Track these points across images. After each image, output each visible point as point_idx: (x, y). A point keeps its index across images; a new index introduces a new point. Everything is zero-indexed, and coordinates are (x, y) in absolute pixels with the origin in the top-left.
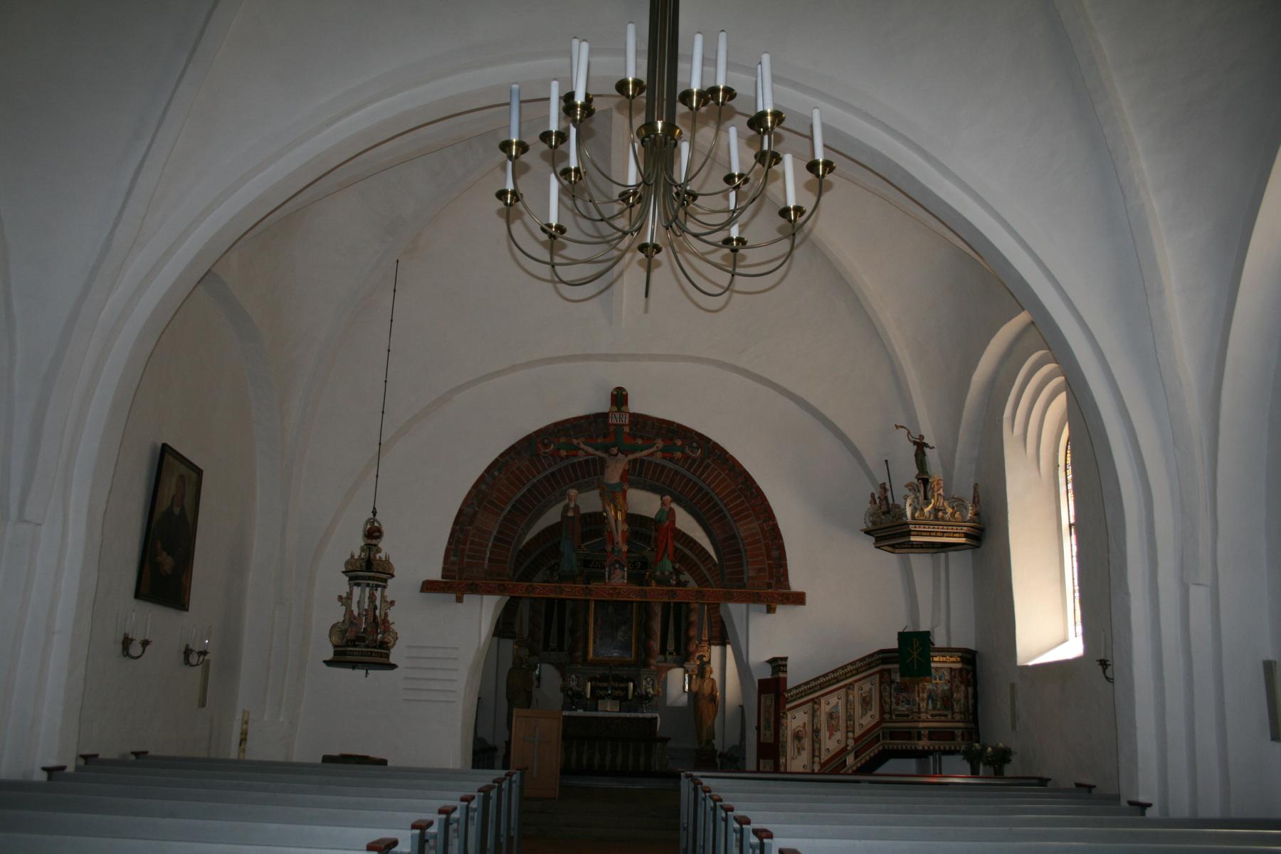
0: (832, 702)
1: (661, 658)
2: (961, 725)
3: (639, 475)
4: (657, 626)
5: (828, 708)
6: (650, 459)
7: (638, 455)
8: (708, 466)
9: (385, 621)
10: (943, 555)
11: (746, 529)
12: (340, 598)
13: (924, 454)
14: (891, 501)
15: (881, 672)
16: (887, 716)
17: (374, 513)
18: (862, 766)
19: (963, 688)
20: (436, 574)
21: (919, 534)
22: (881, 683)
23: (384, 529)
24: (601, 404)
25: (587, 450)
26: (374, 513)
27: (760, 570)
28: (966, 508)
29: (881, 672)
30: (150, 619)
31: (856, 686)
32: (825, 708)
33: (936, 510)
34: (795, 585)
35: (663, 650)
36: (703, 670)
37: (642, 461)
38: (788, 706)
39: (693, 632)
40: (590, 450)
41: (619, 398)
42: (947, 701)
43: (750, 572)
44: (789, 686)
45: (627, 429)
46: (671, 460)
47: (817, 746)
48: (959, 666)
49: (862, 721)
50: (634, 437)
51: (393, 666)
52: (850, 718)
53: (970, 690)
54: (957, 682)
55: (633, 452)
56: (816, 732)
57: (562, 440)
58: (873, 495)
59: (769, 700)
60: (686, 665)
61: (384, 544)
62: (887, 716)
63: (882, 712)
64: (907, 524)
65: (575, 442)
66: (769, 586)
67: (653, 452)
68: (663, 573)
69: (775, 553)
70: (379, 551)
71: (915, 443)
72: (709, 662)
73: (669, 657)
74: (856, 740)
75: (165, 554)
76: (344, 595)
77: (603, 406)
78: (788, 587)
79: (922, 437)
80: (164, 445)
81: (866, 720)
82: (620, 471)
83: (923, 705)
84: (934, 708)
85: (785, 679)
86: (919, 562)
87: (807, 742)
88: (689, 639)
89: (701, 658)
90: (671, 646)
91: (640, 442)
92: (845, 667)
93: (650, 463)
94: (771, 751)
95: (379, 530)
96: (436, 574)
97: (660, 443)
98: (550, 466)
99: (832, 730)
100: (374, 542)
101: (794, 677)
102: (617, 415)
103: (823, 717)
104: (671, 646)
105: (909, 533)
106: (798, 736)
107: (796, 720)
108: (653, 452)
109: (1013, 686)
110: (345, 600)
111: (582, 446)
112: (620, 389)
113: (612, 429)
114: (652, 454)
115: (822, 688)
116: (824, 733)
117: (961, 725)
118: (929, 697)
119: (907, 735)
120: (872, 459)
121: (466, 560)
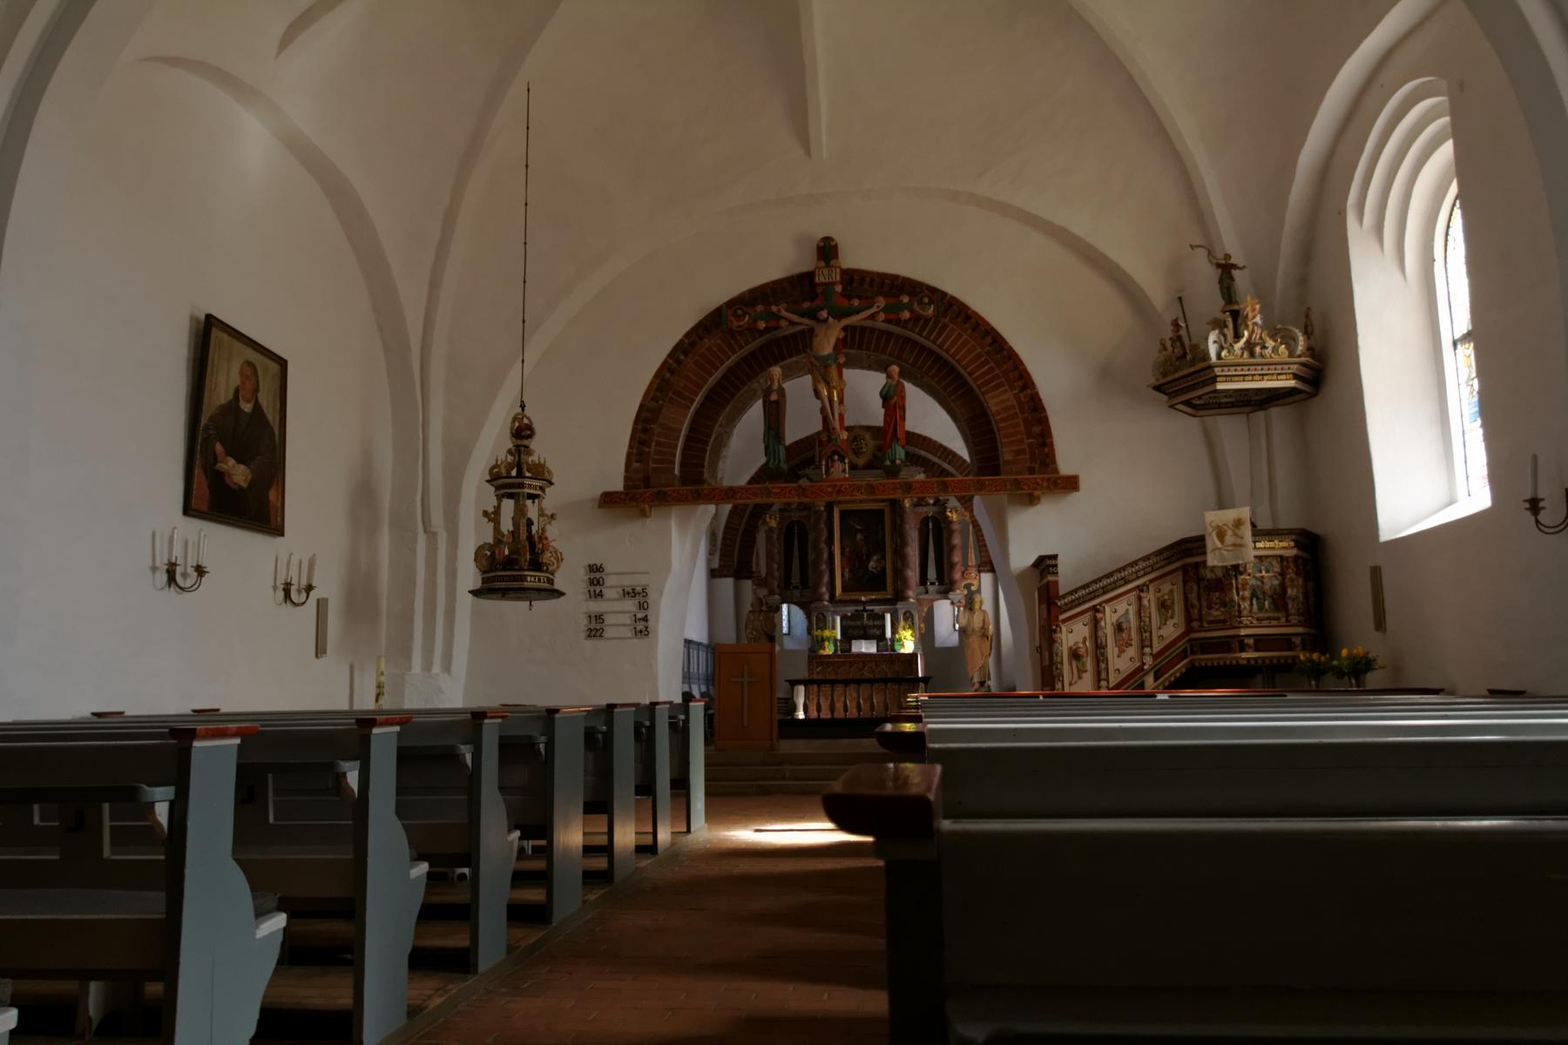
0: (1118, 610)
1: (922, 589)
2: (1300, 630)
3: (862, 347)
4: (913, 552)
5: (1115, 617)
6: (869, 323)
7: (854, 320)
8: (944, 327)
9: (542, 538)
10: (1261, 414)
11: (997, 402)
12: (485, 514)
13: (1232, 278)
14: (1187, 342)
15: (1185, 569)
16: (1195, 624)
17: (523, 407)
18: (1177, 679)
19: (1301, 581)
20: (617, 484)
21: (1229, 378)
22: (1185, 582)
23: (535, 425)
24: (802, 261)
25: (790, 320)
26: (523, 407)
27: (1018, 452)
28: (1295, 339)
29: (1185, 569)
30: (223, 544)
31: (1151, 588)
32: (1109, 618)
33: (1250, 347)
34: (1065, 467)
35: (923, 580)
36: (970, 604)
37: (863, 329)
38: (1062, 617)
39: (957, 558)
40: (794, 318)
41: (827, 250)
42: (1279, 600)
43: (1006, 455)
44: (1061, 592)
45: (839, 288)
46: (898, 322)
48: (1294, 552)
49: (1161, 632)
50: (850, 298)
51: (560, 594)
52: (1144, 629)
53: (1311, 585)
54: (1291, 574)
55: (848, 314)
56: (1099, 647)
57: (759, 308)
60: (951, 595)
61: (534, 444)
62: (1195, 624)
63: (1189, 619)
64: (1211, 367)
65: (774, 308)
66: (1031, 471)
67: (873, 315)
68: (893, 462)
69: (1036, 429)
70: (529, 452)
71: (1219, 266)
72: (979, 591)
73: (931, 588)
74: (1155, 657)
75: (232, 461)
76: (491, 510)
77: (807, 263)
78: (1056, 471)
79: (1228, 256)
80: (209, 317)
81: (1169, 631)
82: (833, 341)
83: (1245, 605)
84: (1261, 609)
85: (1056, 583)
86: (1228, 427)
87: (1089, 663)
88: (952, 566)
89: (968, 586)
90: (932, 574)
91: (856, 302)
92: (1135, 563)
93: (873, 330)
94: (1048, 675)
95: (530, 427)
96: (617, 484)
97: (881, 302)
98: (747, 343)
99: (1122, 646)
100: (525, 442)
101: (1067, 577)
102: (826, 271)
104: (932, 574)
105: (1214, 380)
106: (1075, 655)
107: (1073, 634)
108: (873, 315)
109: (1376, 572)
110: (493, 517)
111: (784, 313)
112: (827, 239)
113: (819, 290)
114: (872, 317)
115: (1104, 593)
116: (1111, 650)
117: (1300, 630)
118: (1253, 595)
119: (1225, 645)
120: (1157, 294)
121: (652, 465)
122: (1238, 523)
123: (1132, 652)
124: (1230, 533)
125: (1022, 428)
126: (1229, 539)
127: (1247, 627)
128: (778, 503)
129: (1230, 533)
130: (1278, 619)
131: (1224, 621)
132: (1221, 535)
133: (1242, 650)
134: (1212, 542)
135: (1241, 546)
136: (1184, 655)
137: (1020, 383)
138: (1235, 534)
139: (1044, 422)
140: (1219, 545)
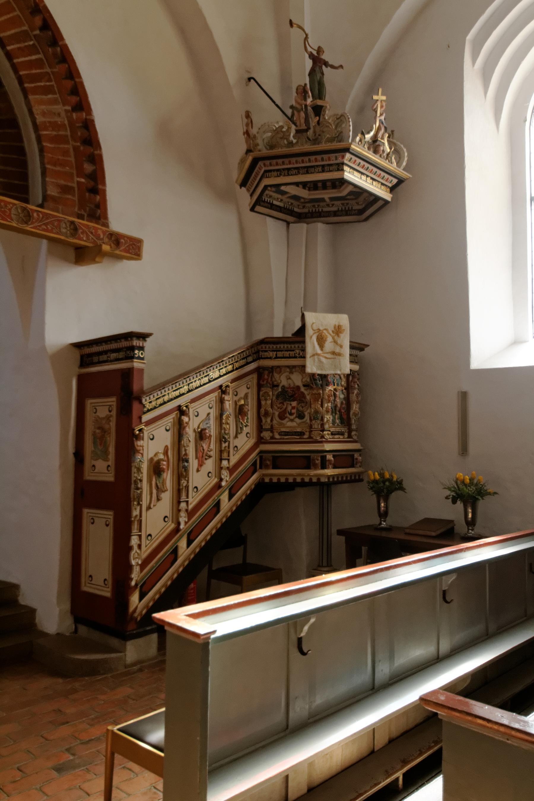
22: (259, 386)
27: (66, 190)
29: (259, 371)
47: (184, 482)
52: (222, 439)
56: (182, 460)
58: (252, 127)
59: (103, 408)
63: (260, 429)
64: (343, 164)
69: (88, 168)
74: (190, 514)
87: (168, 478)
103: (190, 433)
106: (156, 469)
109: (464, 396)
119: (306, 461)
122: (338, 330)
123: (210, 465)
124: (330, 339)
125: (72, 159)
126: (329, 345)
127: (328, 442)
128: (323, 144)
129: (330, 339)
130: (342, 434)
131: (301, 434)
132: (321, 341)
133: (324, 466)
134: (311, 344)
135: (339, 354)
136: (254, 468)
137: (74, 99)
138: (335, 342)
139: (97, 160)
140: (319, 351)
